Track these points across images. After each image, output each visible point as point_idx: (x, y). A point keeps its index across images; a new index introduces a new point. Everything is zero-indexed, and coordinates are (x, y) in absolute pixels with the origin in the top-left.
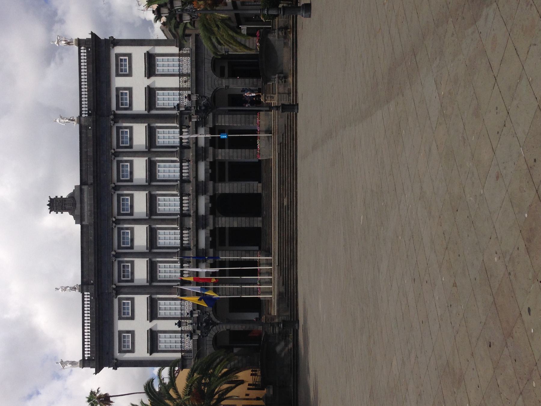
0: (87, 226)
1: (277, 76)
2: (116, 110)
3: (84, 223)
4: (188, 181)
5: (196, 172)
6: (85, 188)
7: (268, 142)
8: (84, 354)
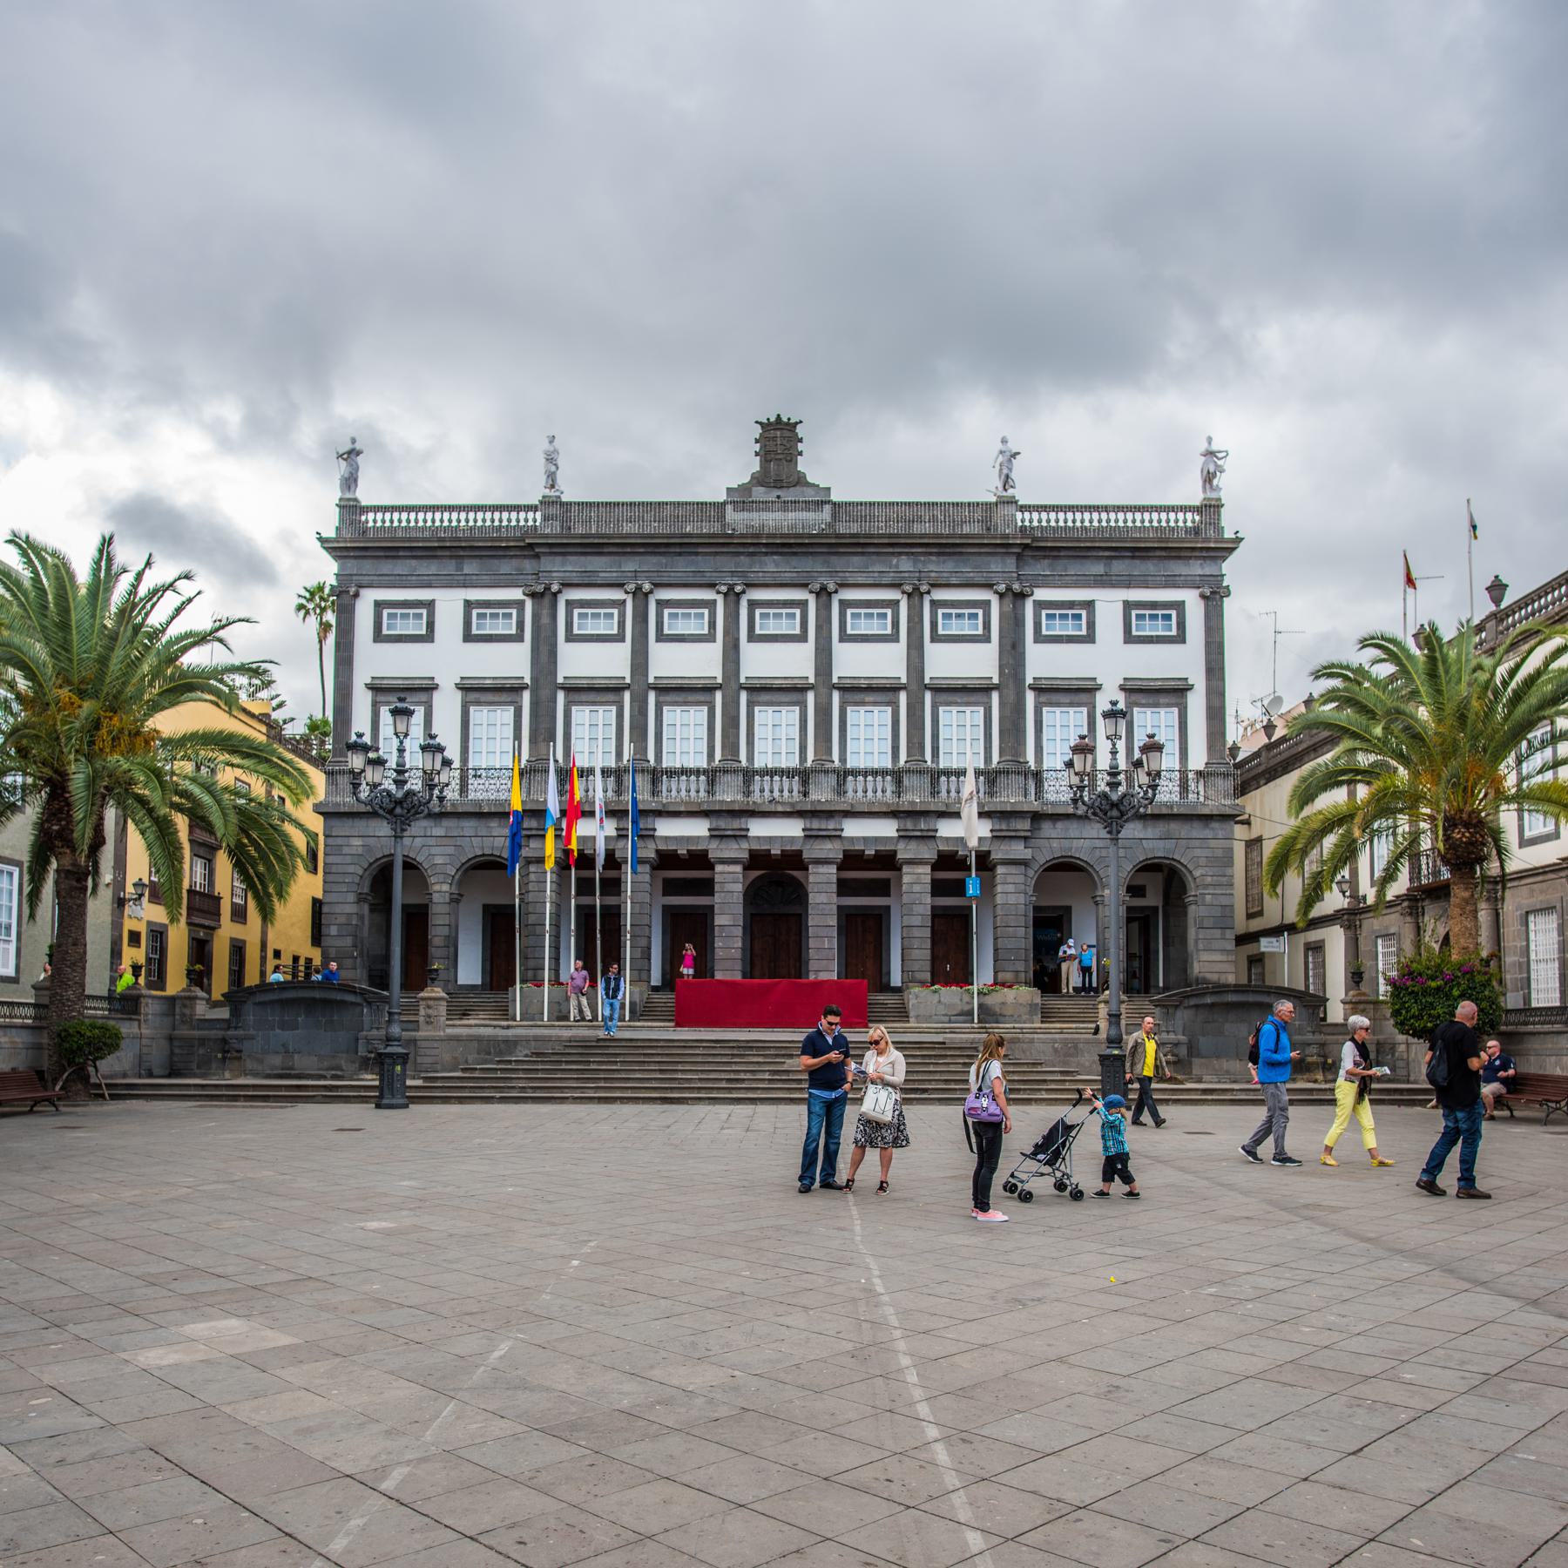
0: (721, 517)
1: (1182, 1038)
2: (1034, 601)
3: (729, 508)
4: (840, 789)
5: (811, 812)
6: (826, 514)
7: (955, 1013)
8: (376, 509)
